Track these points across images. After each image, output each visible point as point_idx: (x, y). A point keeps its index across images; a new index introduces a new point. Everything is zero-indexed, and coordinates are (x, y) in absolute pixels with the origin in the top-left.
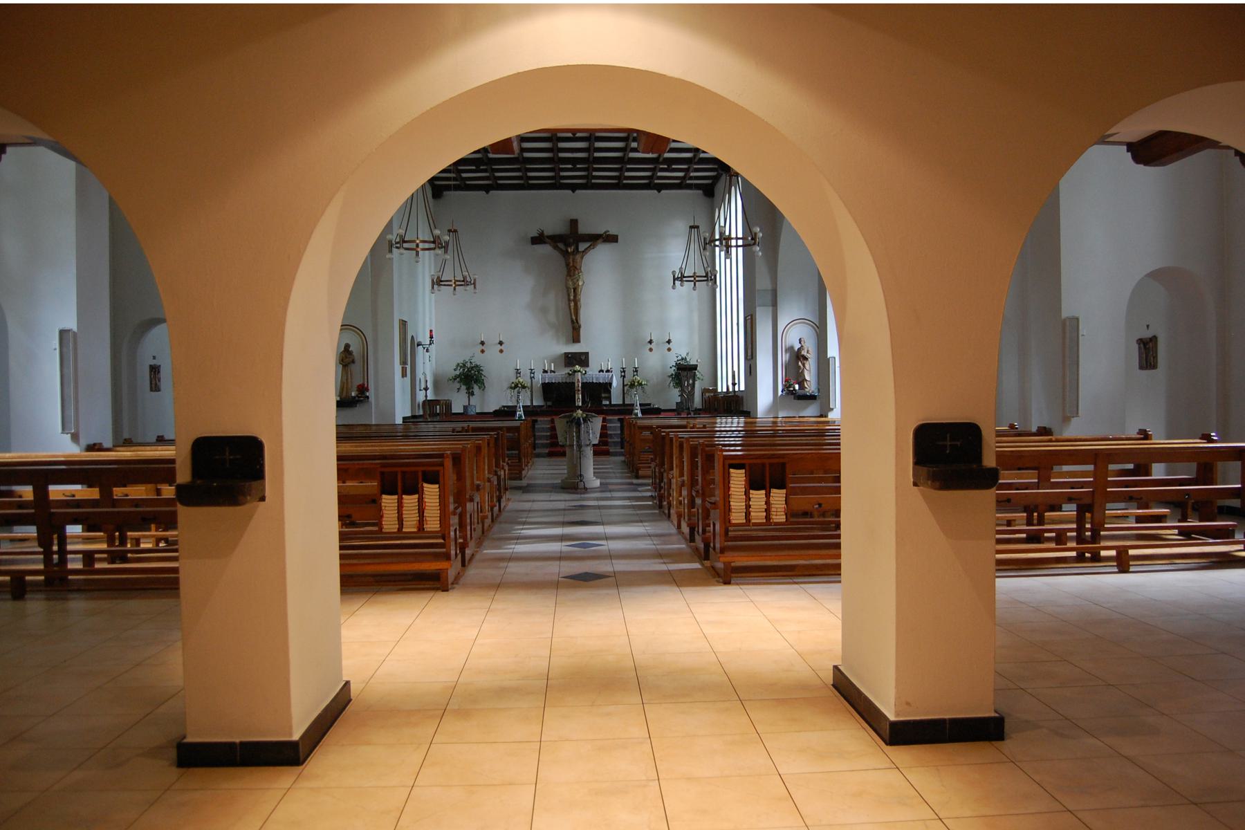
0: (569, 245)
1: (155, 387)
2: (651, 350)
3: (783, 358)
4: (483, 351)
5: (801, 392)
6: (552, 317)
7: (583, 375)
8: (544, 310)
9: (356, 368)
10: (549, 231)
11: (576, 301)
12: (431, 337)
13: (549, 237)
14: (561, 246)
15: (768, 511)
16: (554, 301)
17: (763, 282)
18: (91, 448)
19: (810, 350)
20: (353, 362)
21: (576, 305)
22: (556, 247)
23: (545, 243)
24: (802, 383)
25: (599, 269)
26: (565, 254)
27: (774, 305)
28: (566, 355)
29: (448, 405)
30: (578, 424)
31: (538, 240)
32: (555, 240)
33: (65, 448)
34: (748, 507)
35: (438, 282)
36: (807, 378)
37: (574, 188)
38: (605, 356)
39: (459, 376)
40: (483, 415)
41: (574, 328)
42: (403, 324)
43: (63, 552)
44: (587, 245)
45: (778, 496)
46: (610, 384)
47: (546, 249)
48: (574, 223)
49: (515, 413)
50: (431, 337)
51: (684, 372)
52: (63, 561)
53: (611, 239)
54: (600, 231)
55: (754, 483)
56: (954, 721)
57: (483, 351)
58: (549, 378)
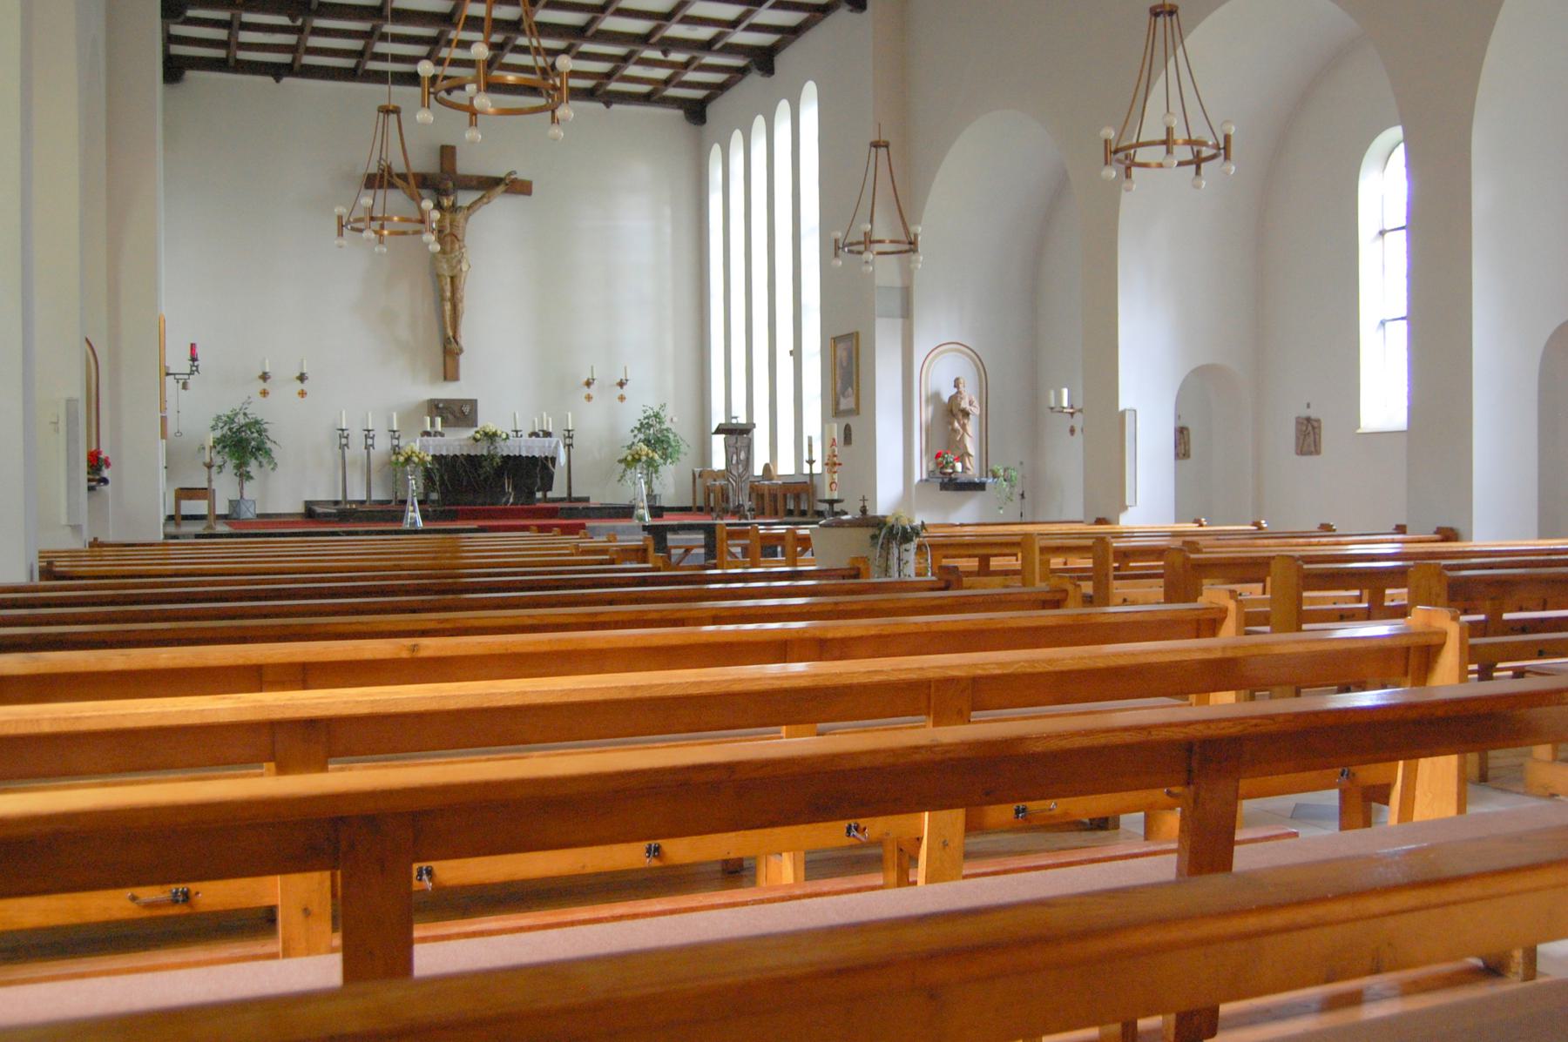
2: (589, 398)
4: (264, 393)
12: (194, 359)
16: (409, 301)
23: (392, 185)
25: (492, 231)
27: (907, 313)
32: (425, 182)
38: (510, 412)
40: (270, 526)
44: (473, 196)
46: (553, 460)
47: (396, 201)
48: (447, 153)
49: (398, 516)
50: (194, 359)
51: (655, 441)
53: (519, 187)
54: (500, 172)
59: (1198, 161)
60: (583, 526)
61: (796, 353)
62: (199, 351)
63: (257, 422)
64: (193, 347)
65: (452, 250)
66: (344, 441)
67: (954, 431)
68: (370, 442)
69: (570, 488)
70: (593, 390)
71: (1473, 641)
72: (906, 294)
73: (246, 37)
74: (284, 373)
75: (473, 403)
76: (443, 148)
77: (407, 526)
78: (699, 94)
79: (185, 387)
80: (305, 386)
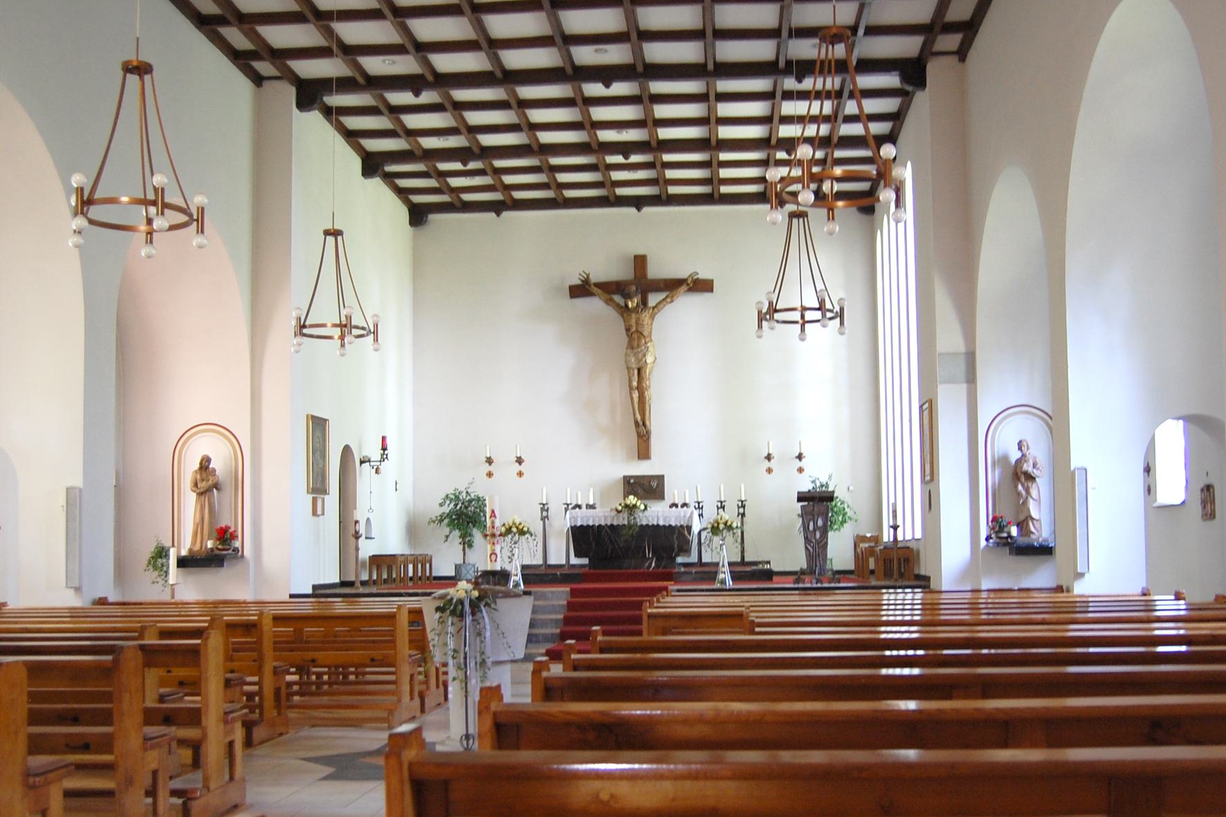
0: (633, 293)
2: (769, 471)
3: (988, 478)
5: (1023, 541)
7: (656, 513)
10: (599, 274)
11: (641, 389)
12: (384, 449)
13: (598, 285)
14: (617, 298)
16: (609, 389)
17: (950, 339)
19: (1039, 452)
22: (609, 302)
23: (591, 294)
24: (1023, 524)
25: (678, 327)
26: (624, 310)
29: (426, 560)
30: (462, 616)
31: (581, 290)
32: (610, 289)
36: (1034, 514)
37: (638, 203)
38: (698, 478)
39: (449, 515)
41: (639, 436)
42: (318, 425)
44: (662, 296)
46: (689, 528)
47: (595, 305)
48: (640, 262)
50: (384, 449)
53: (702, 286)
58: (585, 518)
60: (666, 589)
61: (910, 420)
62: (388, 442)
63: (478, 499)
64: (384, 439)
65: (639, 346)
66: (545, 514)
67: (1019, 494)
68: (741, 510)
69: (743, 552)
70: (772, 464)
72: (970, 357)
73: (725, 173)
74: (505, 458)
75: (660, 478)
76: (636, 257)
77: (718, 586)
78: (864, 186)
79: (377, 471)
80: (522, 468)
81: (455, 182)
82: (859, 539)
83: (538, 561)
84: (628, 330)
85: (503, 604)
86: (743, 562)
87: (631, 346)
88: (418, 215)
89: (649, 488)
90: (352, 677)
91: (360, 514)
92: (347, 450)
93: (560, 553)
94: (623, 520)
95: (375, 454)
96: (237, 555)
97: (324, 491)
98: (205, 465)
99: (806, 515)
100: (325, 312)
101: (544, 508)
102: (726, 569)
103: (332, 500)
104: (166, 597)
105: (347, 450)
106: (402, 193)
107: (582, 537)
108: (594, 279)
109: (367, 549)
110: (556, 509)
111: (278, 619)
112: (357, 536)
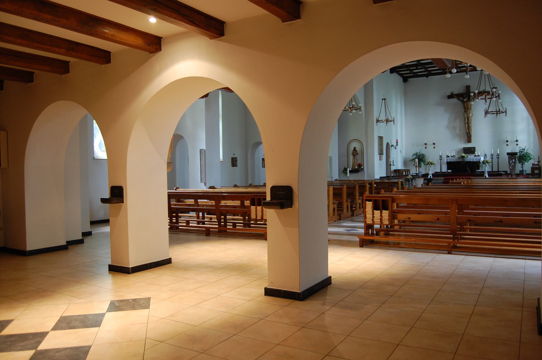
0: (465, 97)
1: (264, 166)
2: (507, 145)
4: (426, 148)
6: (458, 131)
7: (470, 158)
8: (454, 128)
9: (358, 157)
13: (455, 95)
14: (461, 98)
15: (381, 219)
16: (459, 124)
18: (210, 188)
20: (357, 154)
21: (468, 126)
22: (459, 99)
25: (479, 106)
26: (463, 102)
28: (464, 148)
29: (408, 171)
30: (409, 181)
31: (451, 96)
32: (459, 96)
33: (202, 188)
34: (373, 217)
35: (487, 113)
38: (484, 148)
41: (468, 136)
42: (381, 138)
43: (225, 222)
45: (386, 213)
47: (455, 100)
52: (225, 225)
55: (376, 207)
56: (284, 291)
57: (426, 148)
58: (451, 159)
59: (497, 113)
63: (423, 154)
70: (508, 143)
71: (357, 187)
74: (430, 143)
75: (474, 148)
80: (435, 146)
81: (414, 71)
82: (533, 164)
83: (439, 171)
84: (464, 107)
85: (417, 179)
86: (492, 171)
87: (465, 112)
88: (405, 80)
89: (471, 151)
90: (396, 228)
91: (391, 160)
92: (388, 143)
93: (445, 169)
94: (461, 160)
95: (395, 144)
96: (363, 169)
97: (382, 154)
98: (355, 148)
99: (510, 159)
100: (383, 117)
101: (441, 157)
102: (487, 173)
103: (384, 156)
104: (347, 179)
105: (388, 143)
106: (400, 75)
107: (450, 165)
108: (454, 93)
109: (393, 168)
110: (444, 157)
111: (375, 183)
112: (390, 165)
